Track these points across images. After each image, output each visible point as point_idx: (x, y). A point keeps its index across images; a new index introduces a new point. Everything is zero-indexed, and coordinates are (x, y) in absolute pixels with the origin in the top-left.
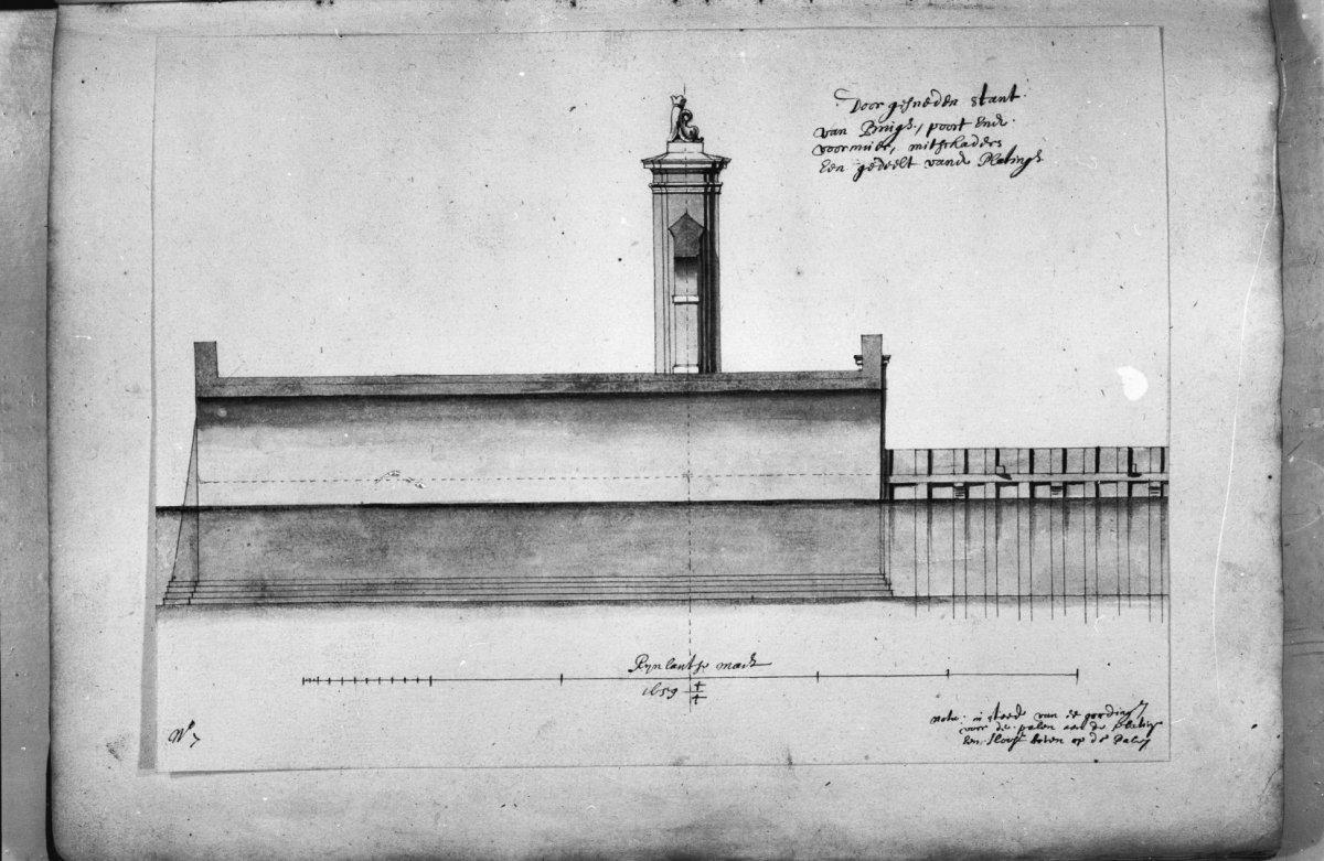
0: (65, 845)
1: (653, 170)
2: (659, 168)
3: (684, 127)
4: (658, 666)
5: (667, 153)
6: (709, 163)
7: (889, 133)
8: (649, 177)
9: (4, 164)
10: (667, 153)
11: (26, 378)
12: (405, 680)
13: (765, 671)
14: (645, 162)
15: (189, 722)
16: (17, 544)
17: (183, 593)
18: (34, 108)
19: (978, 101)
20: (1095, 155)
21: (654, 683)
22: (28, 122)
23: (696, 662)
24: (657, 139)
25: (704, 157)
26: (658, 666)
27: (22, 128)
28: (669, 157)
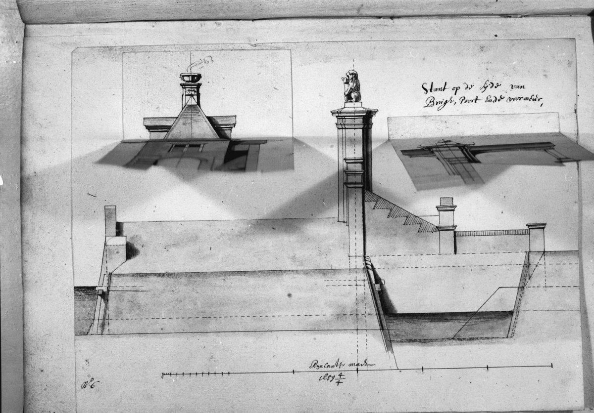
0: (28, 410)
1: (337, 117)
2: (340, 115)
3: (353, 94)
4: (321, 366)
5: (344, 107)
6: (364, 112)
7: (441, 104)
8: (335, 120)
9: (2, 68)
10: (344, 107)
11: (13, 175)
12: (183, 374)
13: (369, 368)
14: (333, 113)
15: (553, 366)
16: (9, 259)
17: (358, 99)
18: (17, 39)
19: (474, 101)
20: (189, 309)
21: (324, 374)
22: (14, 46)
23: (339, 363)
24: (339, 102)
25: (363, 109)
26: (321, 366)
27: (11, 49)
28: (345, 110)
